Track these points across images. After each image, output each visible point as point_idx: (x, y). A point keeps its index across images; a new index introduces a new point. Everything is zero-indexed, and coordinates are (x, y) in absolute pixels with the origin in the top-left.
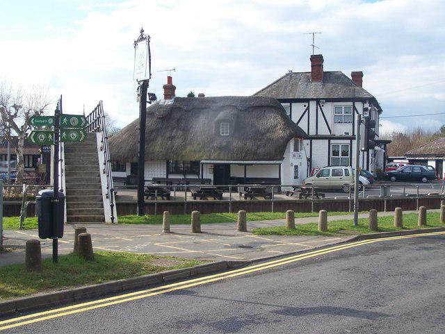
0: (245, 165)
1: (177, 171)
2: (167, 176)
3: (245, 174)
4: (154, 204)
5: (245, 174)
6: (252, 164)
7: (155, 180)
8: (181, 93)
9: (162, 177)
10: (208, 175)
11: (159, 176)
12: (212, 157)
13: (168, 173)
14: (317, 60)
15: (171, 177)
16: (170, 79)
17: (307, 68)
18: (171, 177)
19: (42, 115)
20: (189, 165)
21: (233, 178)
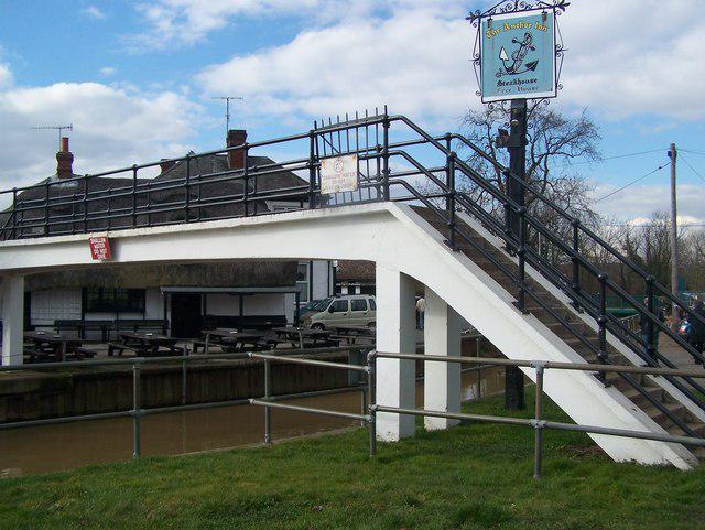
0: (241, 295)
1: (100, 307)
2: (83, 317)
3: (241, 310)
4: (180, 372)
5: (241, 310)
6: (252, 294)
7: (60, 325)
8: (81, 167)
9: (72, 318)
10: (155, 311)
11: (66, 317)
12: (178, 282)
13: (85, 311)
14: (237, 137)
15: (89, 318)
16: (66, 141)
17: (220, 144)
18: (89, 318)
19: (189, 36)
20: (125, 296)
21: (212, 318)
